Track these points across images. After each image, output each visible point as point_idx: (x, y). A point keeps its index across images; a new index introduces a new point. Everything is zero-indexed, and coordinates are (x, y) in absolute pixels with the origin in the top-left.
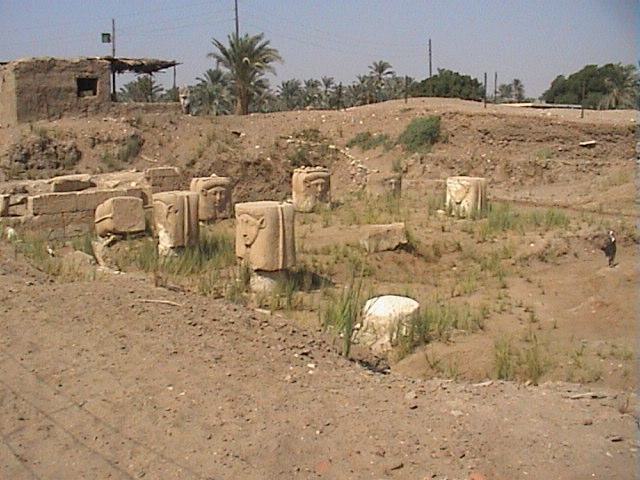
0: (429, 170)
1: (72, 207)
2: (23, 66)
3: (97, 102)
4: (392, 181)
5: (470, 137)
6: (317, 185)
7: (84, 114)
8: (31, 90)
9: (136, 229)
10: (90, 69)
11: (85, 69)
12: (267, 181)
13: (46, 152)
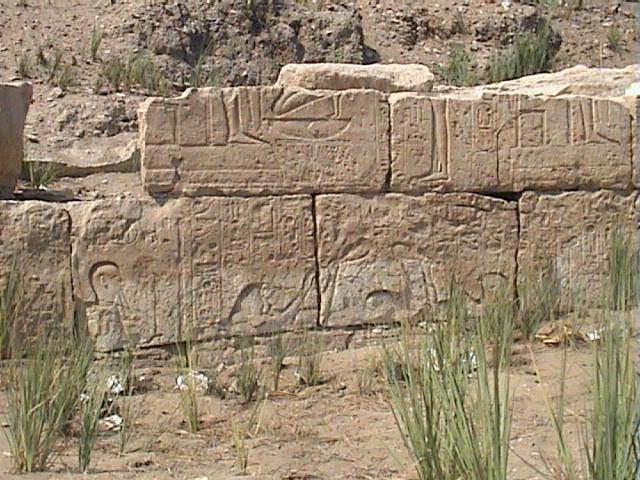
1: (359, 160)
13: (264, 36)
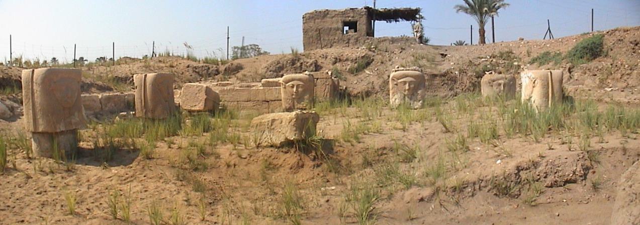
0: (576, 77)
1: (244, 98)
2: (307, 16)
3: (356, 36)
4: (500, 82)
5: (624, 49)
6: (405, 83)
7: (347, 45)
8: (312, 30)
9: (197, 108)
10: (352, 15)
11: (349, 15)
12: (451, 89)
